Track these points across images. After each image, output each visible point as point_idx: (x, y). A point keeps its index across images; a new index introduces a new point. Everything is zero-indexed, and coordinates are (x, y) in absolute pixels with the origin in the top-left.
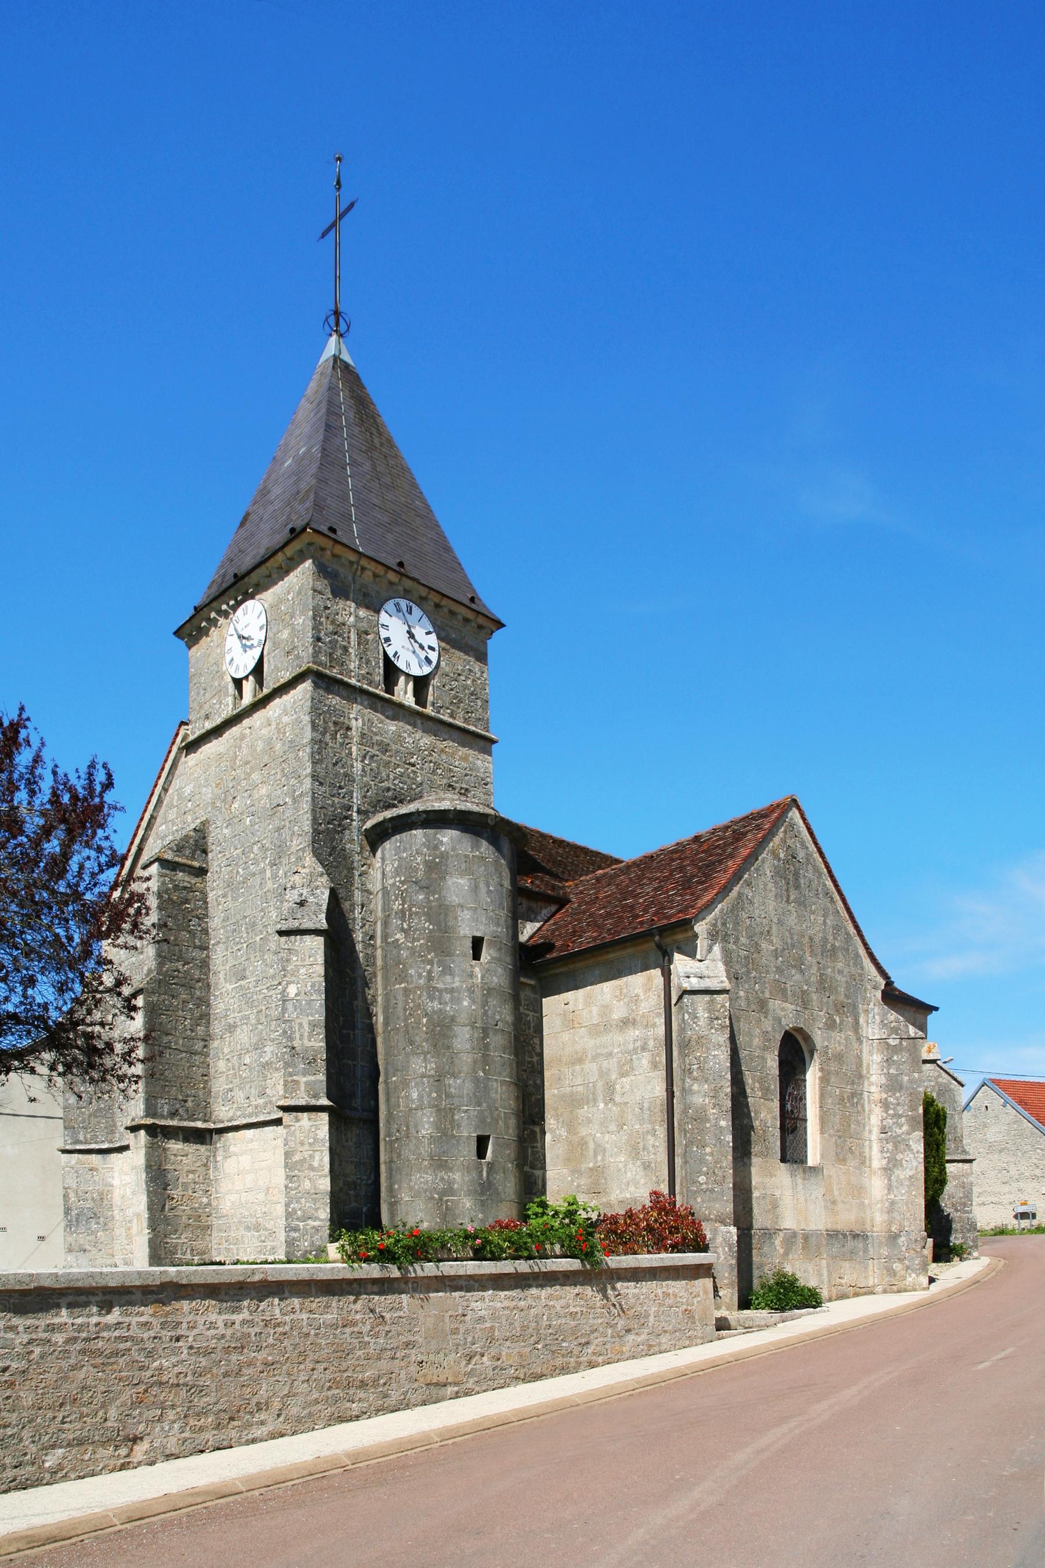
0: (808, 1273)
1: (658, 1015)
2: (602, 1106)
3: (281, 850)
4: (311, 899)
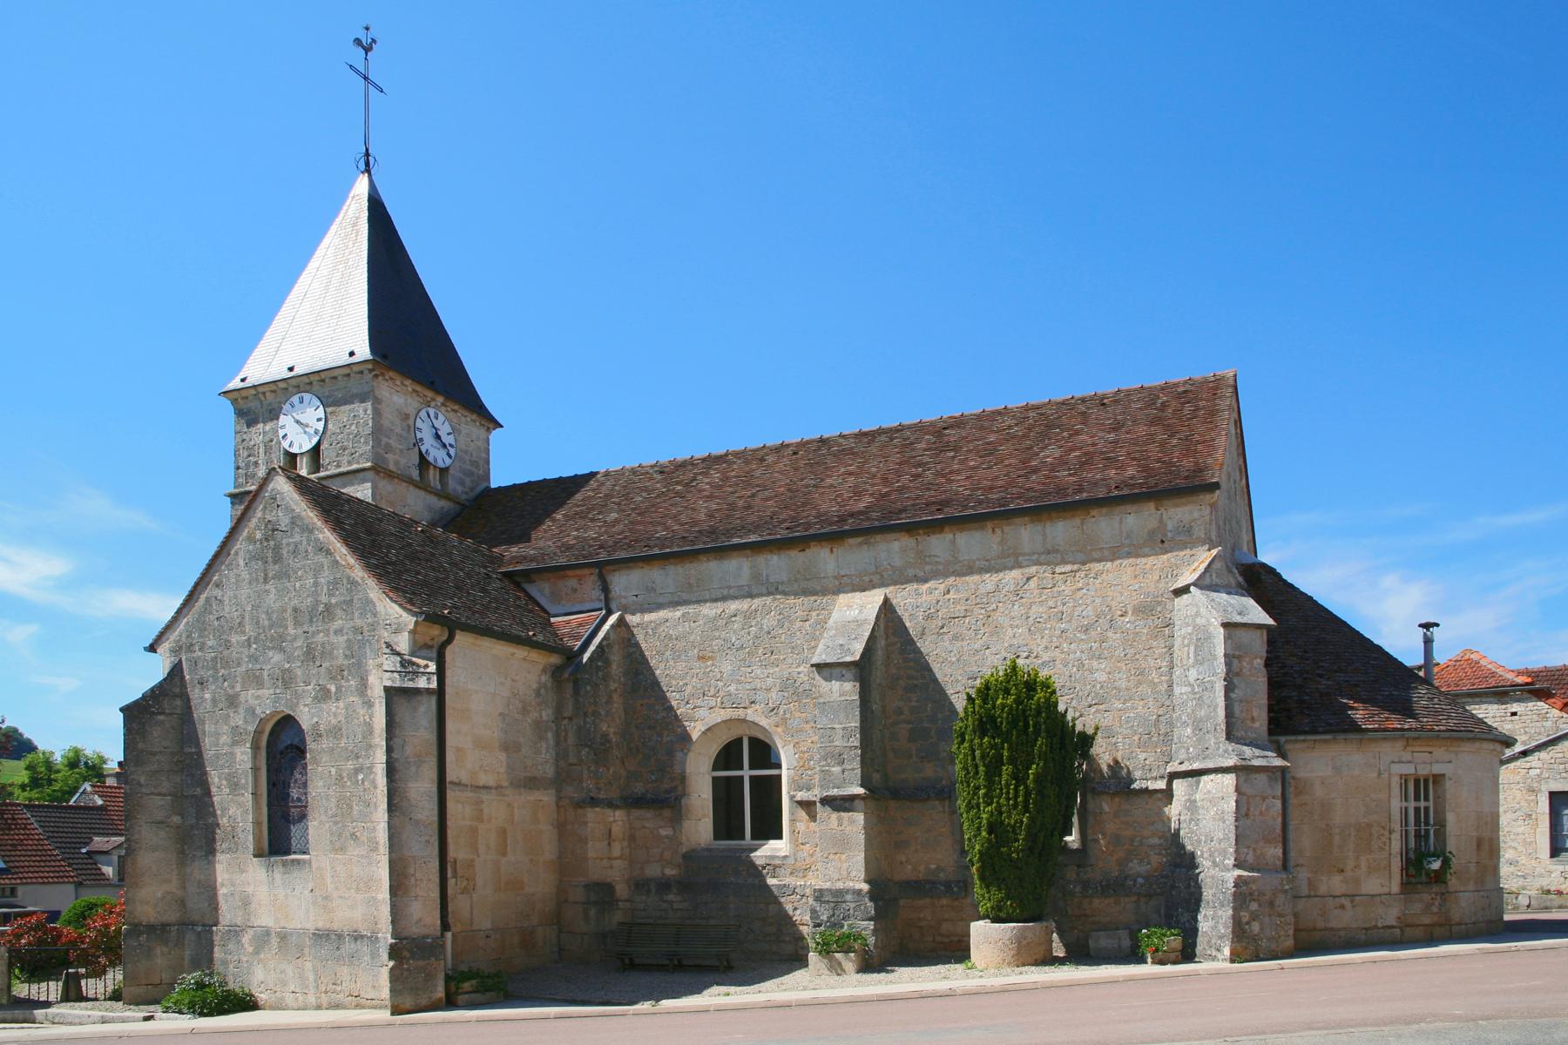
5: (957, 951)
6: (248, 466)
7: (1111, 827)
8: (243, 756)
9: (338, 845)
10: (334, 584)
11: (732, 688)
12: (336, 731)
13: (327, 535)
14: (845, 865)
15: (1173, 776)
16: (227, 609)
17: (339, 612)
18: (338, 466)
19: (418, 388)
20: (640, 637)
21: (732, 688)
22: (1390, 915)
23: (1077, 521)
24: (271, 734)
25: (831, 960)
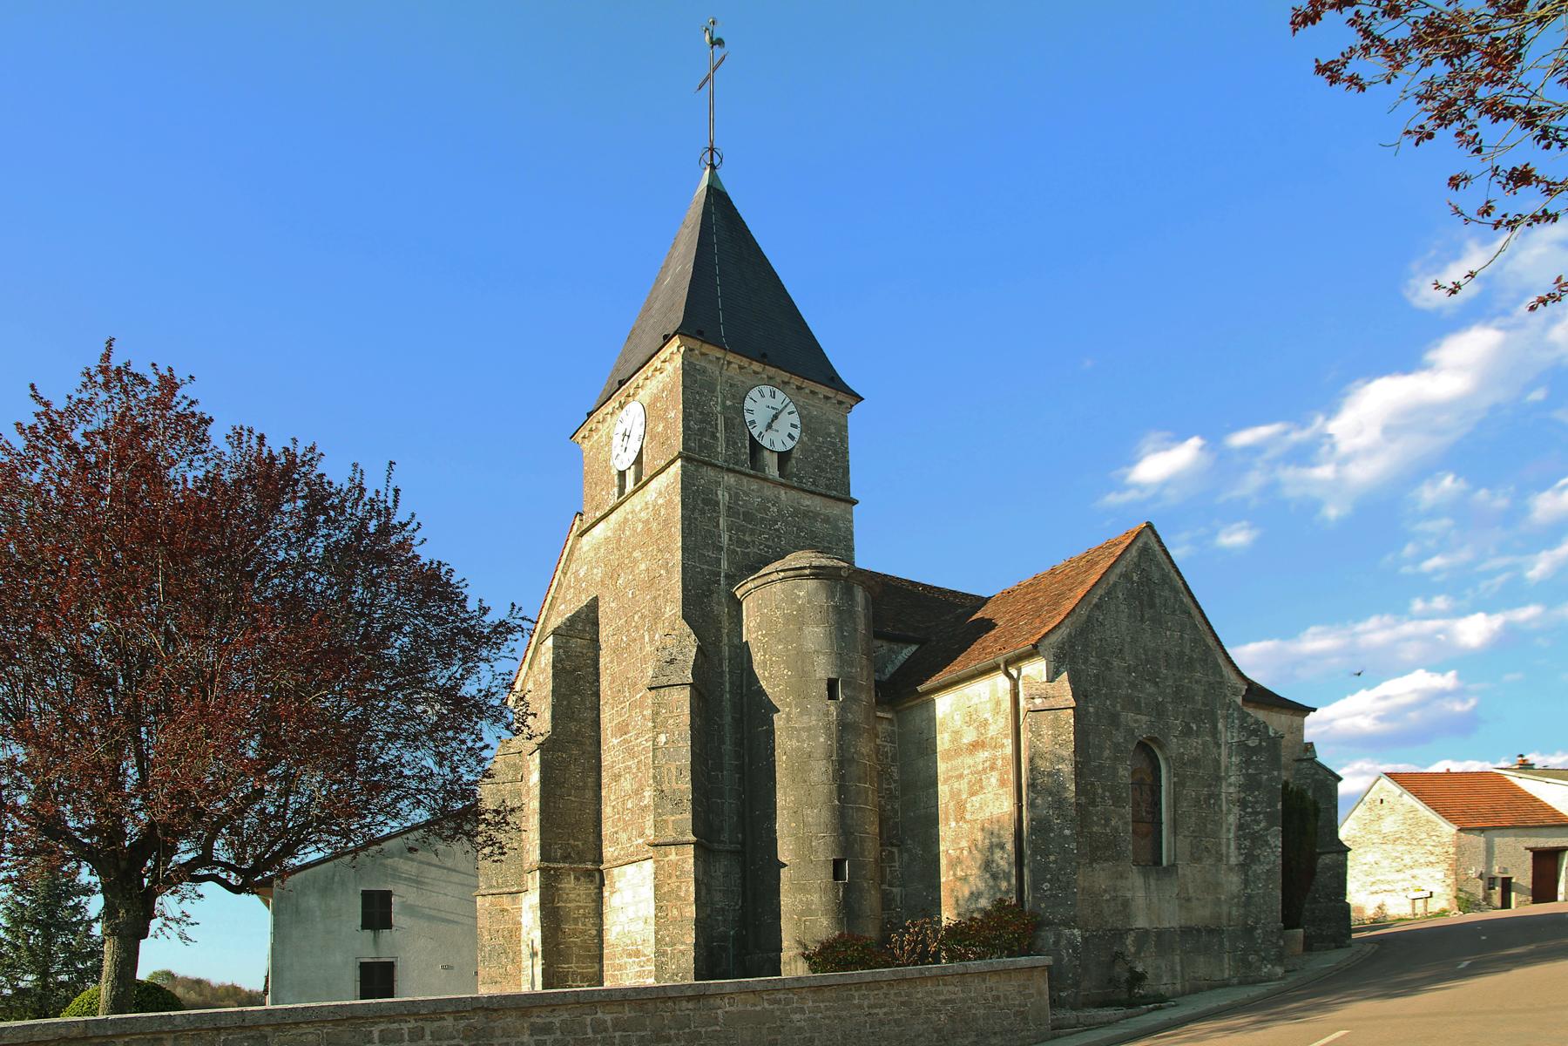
1: (1006, 736)
2: (953, 824)
3: (657, 616)
4: (681, 657)
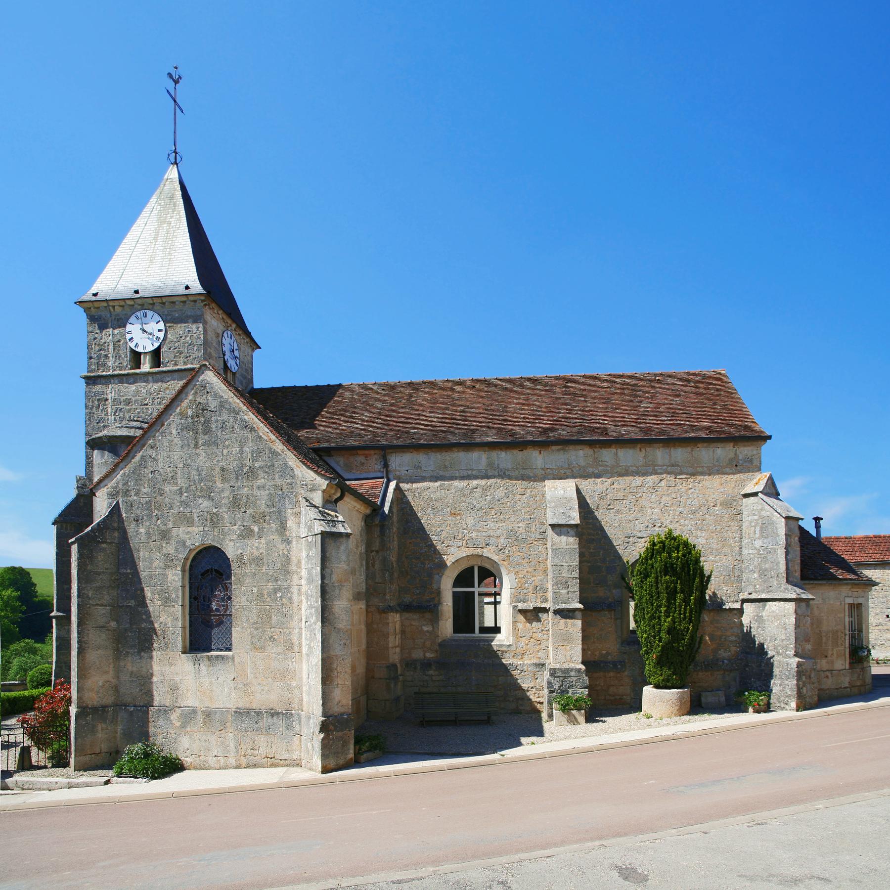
0: (183, 746)
5: (635, 706)
6: (99, 357)
7: (708, 629)
8: (175, 578)
9: (258, 645)
10: (257, 454)
11: (474, 535)
12: (258, 561)
13: (251, 417)
14: (569, 653)
15: (744, 601)
16: (161, 465)
17: (261, 473)
18: (176, 364)
19: (225, 317)
20: (410, 498)
21: (474, 535)
22: (845, 681)
23: (689, 449)
24: (193, 561)
25: (569, 715)
